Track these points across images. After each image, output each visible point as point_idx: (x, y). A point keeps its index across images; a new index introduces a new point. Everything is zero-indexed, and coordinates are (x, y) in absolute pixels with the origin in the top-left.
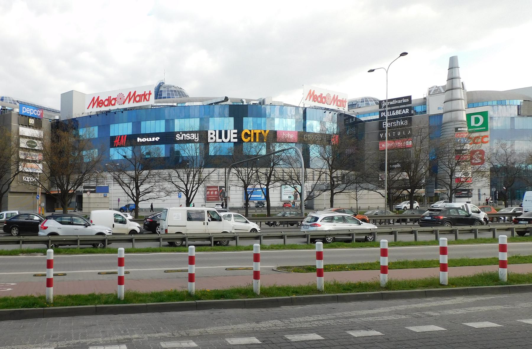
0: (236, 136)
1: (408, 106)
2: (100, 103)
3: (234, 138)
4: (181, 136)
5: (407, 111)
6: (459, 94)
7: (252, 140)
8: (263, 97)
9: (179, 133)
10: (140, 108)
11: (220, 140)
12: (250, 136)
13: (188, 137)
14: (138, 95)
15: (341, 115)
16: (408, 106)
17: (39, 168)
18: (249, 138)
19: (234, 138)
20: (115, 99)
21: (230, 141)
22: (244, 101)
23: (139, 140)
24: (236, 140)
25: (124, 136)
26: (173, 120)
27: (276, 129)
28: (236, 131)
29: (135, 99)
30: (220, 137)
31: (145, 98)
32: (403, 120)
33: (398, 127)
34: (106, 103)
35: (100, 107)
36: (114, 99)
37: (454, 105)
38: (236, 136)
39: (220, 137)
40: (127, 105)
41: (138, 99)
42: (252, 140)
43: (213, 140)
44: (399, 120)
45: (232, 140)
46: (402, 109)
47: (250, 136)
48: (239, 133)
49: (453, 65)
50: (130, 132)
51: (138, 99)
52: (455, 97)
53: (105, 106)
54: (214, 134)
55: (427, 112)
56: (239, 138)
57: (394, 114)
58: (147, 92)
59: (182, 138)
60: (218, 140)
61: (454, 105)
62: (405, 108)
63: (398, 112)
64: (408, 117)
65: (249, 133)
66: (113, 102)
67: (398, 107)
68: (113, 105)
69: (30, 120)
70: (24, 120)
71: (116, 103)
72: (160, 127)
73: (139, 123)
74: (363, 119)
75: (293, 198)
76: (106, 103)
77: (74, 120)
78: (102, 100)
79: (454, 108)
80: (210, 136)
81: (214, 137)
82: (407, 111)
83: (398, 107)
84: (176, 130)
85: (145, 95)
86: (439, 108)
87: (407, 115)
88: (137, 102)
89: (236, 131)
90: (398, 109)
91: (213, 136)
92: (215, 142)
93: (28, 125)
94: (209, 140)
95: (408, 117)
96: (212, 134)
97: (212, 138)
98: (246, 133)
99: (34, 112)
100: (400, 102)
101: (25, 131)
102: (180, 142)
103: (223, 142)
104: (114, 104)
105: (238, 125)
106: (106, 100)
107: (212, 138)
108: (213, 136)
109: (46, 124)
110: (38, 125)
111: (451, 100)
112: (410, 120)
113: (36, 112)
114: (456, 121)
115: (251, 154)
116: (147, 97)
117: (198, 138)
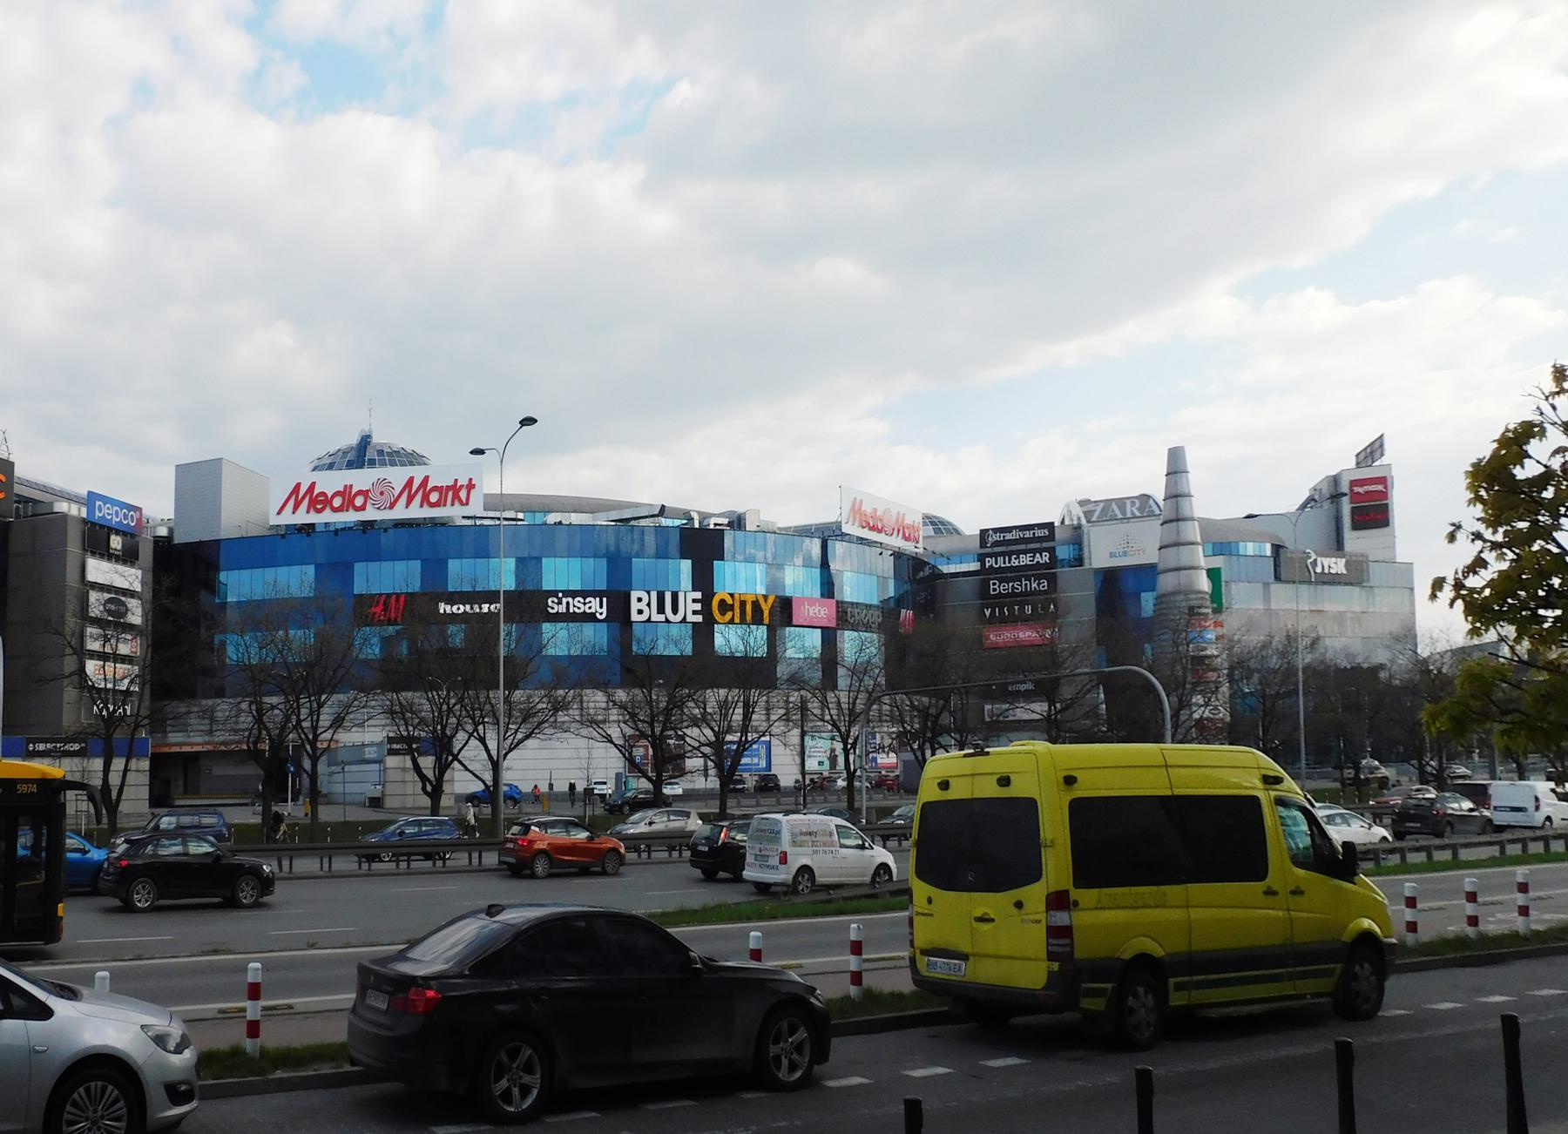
0: (698, 607)
1: (1045, 545)
2: (319, 501)
3: (695, 612)
4: (560, 603)
5: (1046, 558)
6: (1193, 532)
7: (737, 620)
8: (740, 510)
9: (554, 593)
10: (435, 523)
11: (661, 618)
12: (731, 607)
13: (578, 606)
14: (435, 488)
15: (898, 555)
16: (1045, 545)
17: (121, 676)
18: (729, 614)
19: (695, 612)
20: (365, 493)
21: (684, 620)
22: (696, 516)
23: (443, 608)
24: (699, 618)
25: (398, 596)
26: (539, 560)
27: (788, 593)
28: (698, 595)
29: (425, 498)
30: (661, 610)
31: (456, 496)
32: (1038, 578)
33: (1022, 594)
34: (337, 502)
35: (319, 511)
36: (360, 492)
37: (1183, 556)
38: (698, 607)
39: (661, 610)
40: (400, 512)
41: (434, 497)
42: (737, 620)
43: (644, 617)
44: (1028, 578)
45: (691, 618)
46: (1034, 551)
47: (731, 607)
48: (706, 601)
49: (1176, 466)
50: (416, 586)
51: (434, 497)
52: (1183, 538)
53: (335, 510)
54: (645, 600)
55: (1086, 561)
56: (706, 610)
57: (1014, 563)
58: (463, 481)
59: (562, 609)
60: (656, 617)
61: (1183, 556)
62: (1040, 551)
63: (1025, 560)
64: (1048, 572)
65: (730, 601)
66: (359, 501)
67: (1022, 547)
68: (358, 509)
69: (113, 537)
70: (96, 538)
71: (369, 506)
72: (504, 575)
73: (443, 564)
74: (948, 569)
75: (827, 764)
76: (337, 502)
77: (217, 543)
78: (323, 494)
79: (1184, 562)
80: (635, 606)
81: (646, 609)
82: (1046, 558)
83: (1022, 547)
84: (547, 585)
85: (455, 488)
86: (1112, 555)
87: (1046, 566)
88: (433, 505)
89: (698, 595)
90: (1025, 552)
91: (643, 606)
92: (649, 620)
93: (106, 554)
94: (635, 617)
95: (1048, 572)
96: (640, 600)
97: (640, 612)
98: (722, 602)
99: (121, 515)
100: (1028, 534)
101: (98, 570)
102: (558, 618)
103: (667, 621)
104: (363, 508)
105: (703, 581)
106: (337, 494)
107: (640, 612)
108: (643, 606)
109: (146, 552)
110: (128, 557)
111: (1177, 544)
112: (1052, 579)
113: (126, 516)
114: (1189, 591)
115: (654, 653)
116: (463, 494)
117: (604, 610)
